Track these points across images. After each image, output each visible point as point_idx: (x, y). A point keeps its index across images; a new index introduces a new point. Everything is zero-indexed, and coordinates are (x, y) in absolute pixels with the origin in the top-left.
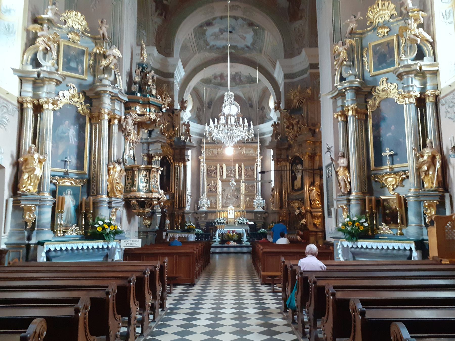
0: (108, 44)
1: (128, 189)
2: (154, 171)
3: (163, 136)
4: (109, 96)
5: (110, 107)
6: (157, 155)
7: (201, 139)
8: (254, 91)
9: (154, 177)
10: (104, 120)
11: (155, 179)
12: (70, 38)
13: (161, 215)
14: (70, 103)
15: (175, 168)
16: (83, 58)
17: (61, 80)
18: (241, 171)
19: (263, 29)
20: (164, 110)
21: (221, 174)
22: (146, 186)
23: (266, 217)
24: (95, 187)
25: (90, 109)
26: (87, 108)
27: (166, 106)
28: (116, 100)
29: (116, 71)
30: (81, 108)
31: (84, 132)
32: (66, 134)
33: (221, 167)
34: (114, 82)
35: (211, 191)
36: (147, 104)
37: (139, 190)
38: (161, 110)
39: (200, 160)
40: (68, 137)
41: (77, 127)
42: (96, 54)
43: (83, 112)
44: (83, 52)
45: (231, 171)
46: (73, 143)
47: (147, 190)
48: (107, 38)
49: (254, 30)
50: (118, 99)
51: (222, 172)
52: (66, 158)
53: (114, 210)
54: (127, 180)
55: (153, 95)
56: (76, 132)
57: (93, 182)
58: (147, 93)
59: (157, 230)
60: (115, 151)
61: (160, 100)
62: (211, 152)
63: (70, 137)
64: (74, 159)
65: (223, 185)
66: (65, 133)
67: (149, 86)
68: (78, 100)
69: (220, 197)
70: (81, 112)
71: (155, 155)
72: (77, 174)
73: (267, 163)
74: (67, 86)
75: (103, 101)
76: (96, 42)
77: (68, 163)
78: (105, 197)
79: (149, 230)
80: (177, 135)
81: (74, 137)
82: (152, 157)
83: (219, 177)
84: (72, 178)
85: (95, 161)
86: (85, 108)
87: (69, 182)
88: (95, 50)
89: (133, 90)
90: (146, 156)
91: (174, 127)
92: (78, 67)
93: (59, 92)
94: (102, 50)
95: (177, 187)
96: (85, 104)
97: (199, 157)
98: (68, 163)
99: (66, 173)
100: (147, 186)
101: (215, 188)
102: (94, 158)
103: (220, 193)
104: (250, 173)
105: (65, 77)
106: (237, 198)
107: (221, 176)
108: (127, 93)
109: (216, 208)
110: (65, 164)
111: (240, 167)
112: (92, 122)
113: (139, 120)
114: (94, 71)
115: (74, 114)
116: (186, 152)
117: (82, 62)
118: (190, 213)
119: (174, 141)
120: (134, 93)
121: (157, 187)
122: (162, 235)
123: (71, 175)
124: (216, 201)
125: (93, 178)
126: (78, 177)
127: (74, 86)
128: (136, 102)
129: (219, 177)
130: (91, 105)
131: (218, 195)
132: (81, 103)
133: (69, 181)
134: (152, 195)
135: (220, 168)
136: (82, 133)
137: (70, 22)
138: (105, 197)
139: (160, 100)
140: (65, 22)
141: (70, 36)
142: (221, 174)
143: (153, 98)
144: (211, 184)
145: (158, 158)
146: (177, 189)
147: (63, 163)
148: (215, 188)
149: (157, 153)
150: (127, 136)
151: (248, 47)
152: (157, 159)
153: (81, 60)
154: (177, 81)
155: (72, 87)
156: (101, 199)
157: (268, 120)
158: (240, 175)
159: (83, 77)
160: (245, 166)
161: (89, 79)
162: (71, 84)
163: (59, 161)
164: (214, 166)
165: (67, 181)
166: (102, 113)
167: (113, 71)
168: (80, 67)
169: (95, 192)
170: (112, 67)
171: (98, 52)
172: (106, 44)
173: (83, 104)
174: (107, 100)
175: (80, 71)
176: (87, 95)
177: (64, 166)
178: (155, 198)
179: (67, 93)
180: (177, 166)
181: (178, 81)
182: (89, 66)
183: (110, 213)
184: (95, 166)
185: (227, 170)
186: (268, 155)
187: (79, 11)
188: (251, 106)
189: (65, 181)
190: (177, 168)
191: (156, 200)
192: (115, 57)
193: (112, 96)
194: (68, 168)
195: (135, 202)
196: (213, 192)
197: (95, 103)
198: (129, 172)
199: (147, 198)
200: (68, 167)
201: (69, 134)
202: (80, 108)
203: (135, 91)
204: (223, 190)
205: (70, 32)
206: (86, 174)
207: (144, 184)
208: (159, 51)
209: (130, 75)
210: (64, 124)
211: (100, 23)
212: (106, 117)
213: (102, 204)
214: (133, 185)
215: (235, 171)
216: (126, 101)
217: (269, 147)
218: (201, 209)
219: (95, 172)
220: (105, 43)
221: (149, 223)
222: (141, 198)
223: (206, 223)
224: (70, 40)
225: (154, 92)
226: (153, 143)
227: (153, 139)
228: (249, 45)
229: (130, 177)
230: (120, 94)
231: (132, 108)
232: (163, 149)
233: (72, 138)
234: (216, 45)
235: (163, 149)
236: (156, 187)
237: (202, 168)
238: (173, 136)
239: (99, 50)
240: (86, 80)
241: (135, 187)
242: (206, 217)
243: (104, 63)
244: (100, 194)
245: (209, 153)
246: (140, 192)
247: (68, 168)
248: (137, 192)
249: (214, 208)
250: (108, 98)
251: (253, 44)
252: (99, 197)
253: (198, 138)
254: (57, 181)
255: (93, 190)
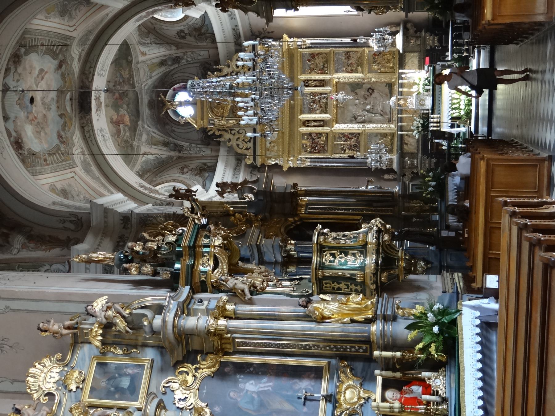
0: (85, 320)
1: (359, 288)
2: (324, 240)
3: (247, 234)
4: (183, 319)
5: (203, 317)
6: (286, 246)
7: (246, 165)
8: (145, 54)
9: (336, 241)
10: (228, 327)
11: (340, 239)
12: (77, 387)
13: (407, 240)
14: (197, 388)
15: (310, 213)
16: (112, 365)
17: (156, 401)
18: (315, 80)
19: (26, 32)
20: (204, 221)
21: (321, 123)
22: (354, 255)
23: (415, 27)
24: (354, 347)
25: (207, 353)
26: (204, 360)
27: (196, 217)
28: (190, 306)
29: (136, 306)
30: (205, 370)
31: (250, 365)
32: (255, 396)
33: (306, 123)
34: (159, 309)
35: (355, 146)
36: (194, 251)
37: (362, 268)
38: (204, 227)
39: (290, 167)
40: (259, 393)
41: (240, 378)
42: (103, 343)
43: (214, 366)
44: (101, 365)
45: (314, 102)
46: (271, 384)
47: (362, 253)
48: (73, 322)
49: (27, 53)
50: (188, 302)
51: (315, 121)
52: (299, 398)
53: (400, 312)
54: (341, 290)
55: (177, 240)
56: (250, 380)
57: (345, 350)
58: (173, 252)
59: (437, 248)
60: (284, 310)
61: (185, 229)
62: (272, 145)
63: (260, 390)
64: (301, 383)
65: (344, 121)
66: (253, 398)
67: (159, 248)
68: (191, 374)
69: (372, 126)
70: (213, 369)
71: (286, 251)
72: (331, 378)
73: (296, 24)
74: (164, 393)
75: (192, 330)
76: (82, 343)
77: (309, 394)
78: (375, 327)
79: (436, 263)
80: (244, 208)
81: (260, 383)
82: (289, 256)
83: (327, 129)
84: (338, 387)
85: (305, 347)
86: (204, 363)
87: (345, 393)
88: (98, 344)
89: (168, 276)
90: (287, 268)
91: (227, 214)
92: (129, 374)
93: (178, 408)
94: (96, 331)
95: (349, 209)
96: (198, 363)
97: (285, 169)
98: (309, 394)
99: (328, 399)
100: (353, 254)
101: (350, 136)
102: (300, 348)
103: (361, 126)
104: (319, 61)
105: (149, 394)
106: (373, 90)
107: (324, 123)
108: (174, 288)
109: (393, 135)
110: (311, 400)
111: (307, 83)
112: (231, 351)
113: (225, 267)
114: (136, 347)
115: (216, 384)
116: (277, 191)
117: (119, 368)
118: (404, 183)
119: (256, 215)
120: (175, 276)
121: (355, 235)
122: (448, 237)
123: (331, 391)
124: (377, 135)
125: (338, 350)
126: (335, 376)
127: (165, 381)
128: (191, 268)
129: (327, 129)
130: (201, 352)
131: (365, 130)
132: (196, 369)
133: (343, 393)
134: (371, 244)
135: (308, 126)
136: (252, 369)
137: (50, 387)
138: (374, 328)
139: (185, 229)
140: (50, 395)
141: (73, 387)
142: (321, 123)
143: (184, 239)
144: (341, 145)
145: (291, 244)
146: (353, 210)
147: (308, 403)
148: (350, 136)
149: (281, 247)
150: (254, 290)
151: (60, 66)
152: (293, 248)
153: (116, 368)
154: (135, 208)
155: (166, 385)
156: (379, 333)
157: (206, 23)
158: (322, 83)
159: (147, 365)
160: (304, 72)
161: (150, 354)
162: (162, 386)
163: (305, 409)
164: (303, 139)
165: (343, 395)
166: (216, 329)
167: (135, 311)
168: (130, 371)
169: (364, 347)
170: (128, 311)
171: (100, 338)
172: (86, 324)
173: (198, 366)
174: (190, 322)
175: (136, 371)
176: (180, 359)
177: (313, 403)
178: (378, 238)
179: (179, 395)
180: (306, 209)
181: (136, 205)
182: (126, 355)
183: (405, 319)
184: (314, 346)
185: (311, 111)
186: (281, 23)
187: (27, 371)
188: (177, 60)
189: (342, 398)
190: (310, 208)
191: (381, 237)
192: (108, 308)
193: (183, 313)
194: (320, 395)
195: (385, 274)
196: (358, 141)
197: (195, 344)
198: (326, 287)
199: (378, 253)
200: (316, 395)
201: (253, 392)
202: (205, 372)
203: (172, 273)
204: (355, 119)
205: (66, 387)
206: (329, 362)
207: (350, 258)
208: (78, 241)
209: (137, 284)
210: (236, 399)
211: (47, 334)
212: (222, 322)
213: (388, 333)
214: (351, 279)
215: (313, 94)
216: (190, 288)
217: (269, 18)
218: (395, 166)
219: (325, 347)
220: (82, 326)
221: (422, 263)
222: (376, 263)
223: (425, 157)
224: (81, 386)
225: (171, 238)
226: (261, 253)
227: (253, 254)
228: (56, 62)
229: (336, 285)
230: (179, 298)
231: (203, 278)
232: (272, 235)
233: (262, 385)
234: (58, 132)
235: (272, 235)
236: (354, 237)
237: (308, 164)
238: (245, 216)
239: (96, 336)
240: (153, 360)
241: (354, 275)
242: (412, 156)
243: (121, 324)
244: (369, 337)
245: (276, 148)
246: (365, 266)
247: (320, 395)
248: (365, 271)
249: (392, 139)
250: (187, 320)
251: (54, 55)
252: (373, 338)
253: (245, 170)
254: (343, 412)
255: (361, 350)
